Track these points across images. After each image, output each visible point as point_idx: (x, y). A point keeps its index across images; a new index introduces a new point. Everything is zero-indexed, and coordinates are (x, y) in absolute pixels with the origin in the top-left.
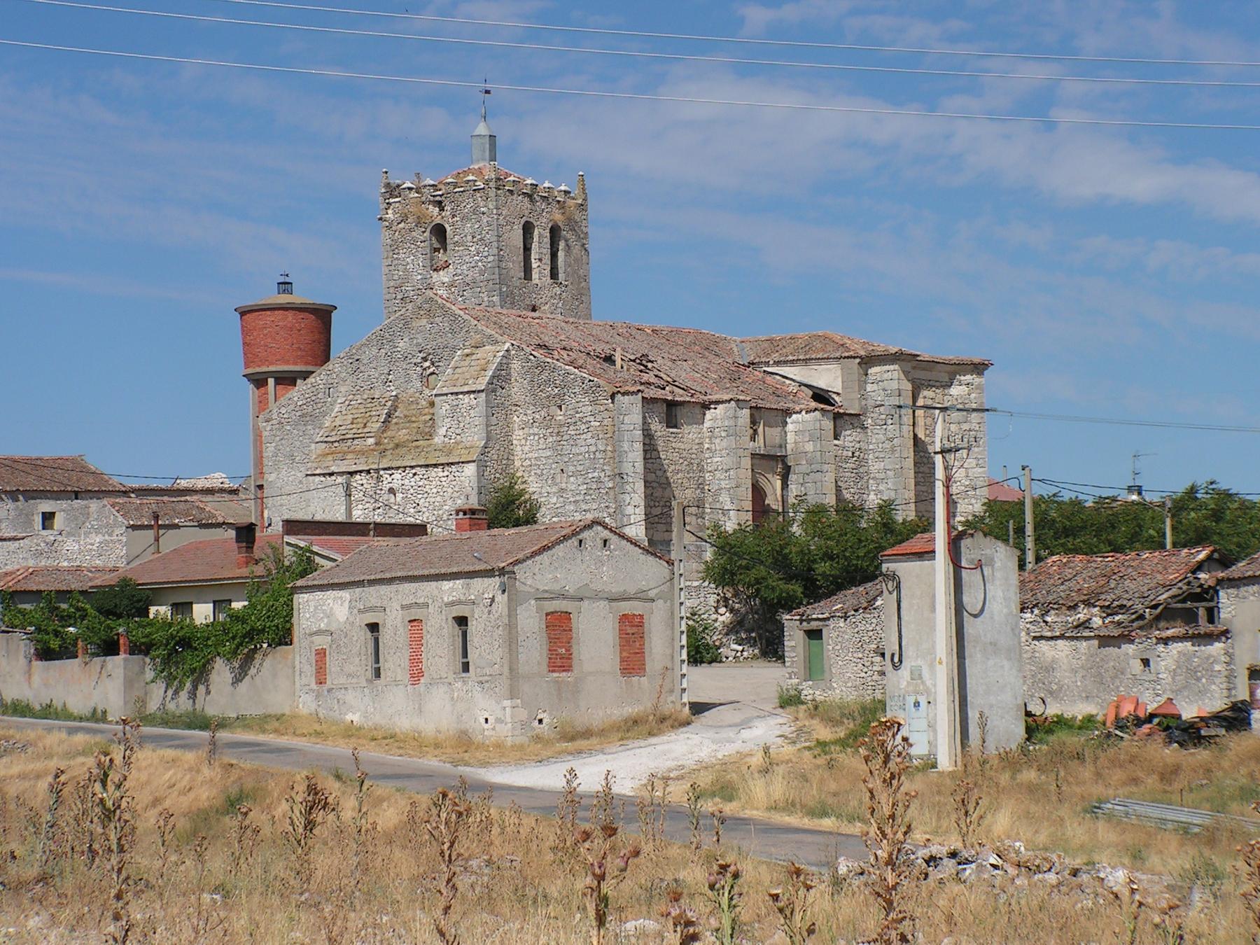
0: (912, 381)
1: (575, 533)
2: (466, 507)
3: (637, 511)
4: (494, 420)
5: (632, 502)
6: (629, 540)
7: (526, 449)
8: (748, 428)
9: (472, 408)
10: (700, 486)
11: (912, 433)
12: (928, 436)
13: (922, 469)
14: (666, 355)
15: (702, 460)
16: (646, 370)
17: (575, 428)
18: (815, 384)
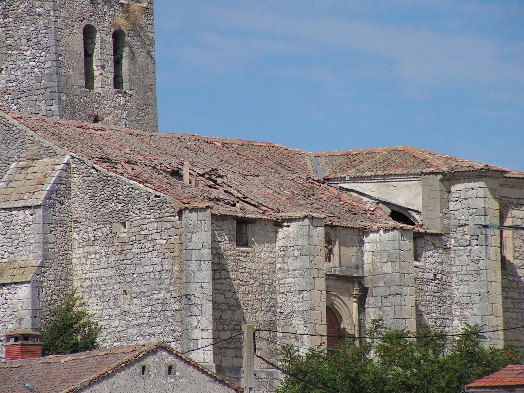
0: (500, 199)
1: (137, 360)
2: (18, 332)
3: (205, 335)
4: (51, 238)
5: (199, 325)
6: (196, 366)
7: (87, 268)
8: (323, 248)
9: (27, 224)
10: (272, 308)
11: (499, 255)
12: (517, 258)
13: (510, 295)
14: (236, 170)
15: (273, 281)
16: (215, 185)
17: (139, 246)
18: (393, 201)
